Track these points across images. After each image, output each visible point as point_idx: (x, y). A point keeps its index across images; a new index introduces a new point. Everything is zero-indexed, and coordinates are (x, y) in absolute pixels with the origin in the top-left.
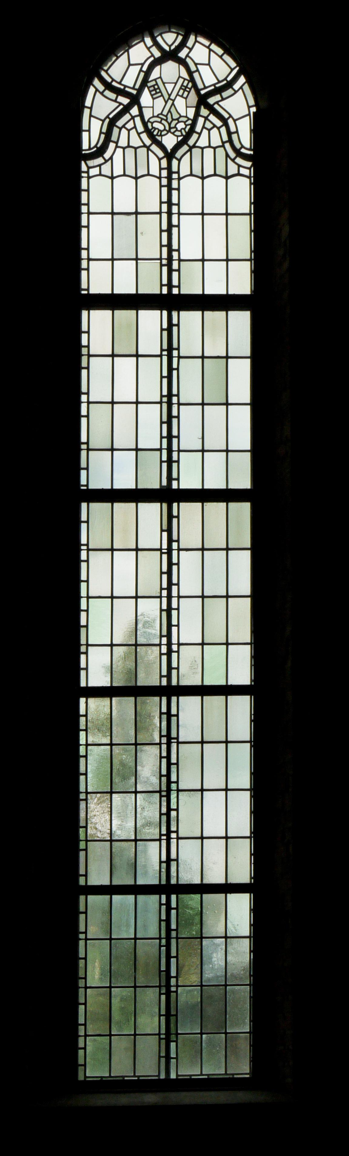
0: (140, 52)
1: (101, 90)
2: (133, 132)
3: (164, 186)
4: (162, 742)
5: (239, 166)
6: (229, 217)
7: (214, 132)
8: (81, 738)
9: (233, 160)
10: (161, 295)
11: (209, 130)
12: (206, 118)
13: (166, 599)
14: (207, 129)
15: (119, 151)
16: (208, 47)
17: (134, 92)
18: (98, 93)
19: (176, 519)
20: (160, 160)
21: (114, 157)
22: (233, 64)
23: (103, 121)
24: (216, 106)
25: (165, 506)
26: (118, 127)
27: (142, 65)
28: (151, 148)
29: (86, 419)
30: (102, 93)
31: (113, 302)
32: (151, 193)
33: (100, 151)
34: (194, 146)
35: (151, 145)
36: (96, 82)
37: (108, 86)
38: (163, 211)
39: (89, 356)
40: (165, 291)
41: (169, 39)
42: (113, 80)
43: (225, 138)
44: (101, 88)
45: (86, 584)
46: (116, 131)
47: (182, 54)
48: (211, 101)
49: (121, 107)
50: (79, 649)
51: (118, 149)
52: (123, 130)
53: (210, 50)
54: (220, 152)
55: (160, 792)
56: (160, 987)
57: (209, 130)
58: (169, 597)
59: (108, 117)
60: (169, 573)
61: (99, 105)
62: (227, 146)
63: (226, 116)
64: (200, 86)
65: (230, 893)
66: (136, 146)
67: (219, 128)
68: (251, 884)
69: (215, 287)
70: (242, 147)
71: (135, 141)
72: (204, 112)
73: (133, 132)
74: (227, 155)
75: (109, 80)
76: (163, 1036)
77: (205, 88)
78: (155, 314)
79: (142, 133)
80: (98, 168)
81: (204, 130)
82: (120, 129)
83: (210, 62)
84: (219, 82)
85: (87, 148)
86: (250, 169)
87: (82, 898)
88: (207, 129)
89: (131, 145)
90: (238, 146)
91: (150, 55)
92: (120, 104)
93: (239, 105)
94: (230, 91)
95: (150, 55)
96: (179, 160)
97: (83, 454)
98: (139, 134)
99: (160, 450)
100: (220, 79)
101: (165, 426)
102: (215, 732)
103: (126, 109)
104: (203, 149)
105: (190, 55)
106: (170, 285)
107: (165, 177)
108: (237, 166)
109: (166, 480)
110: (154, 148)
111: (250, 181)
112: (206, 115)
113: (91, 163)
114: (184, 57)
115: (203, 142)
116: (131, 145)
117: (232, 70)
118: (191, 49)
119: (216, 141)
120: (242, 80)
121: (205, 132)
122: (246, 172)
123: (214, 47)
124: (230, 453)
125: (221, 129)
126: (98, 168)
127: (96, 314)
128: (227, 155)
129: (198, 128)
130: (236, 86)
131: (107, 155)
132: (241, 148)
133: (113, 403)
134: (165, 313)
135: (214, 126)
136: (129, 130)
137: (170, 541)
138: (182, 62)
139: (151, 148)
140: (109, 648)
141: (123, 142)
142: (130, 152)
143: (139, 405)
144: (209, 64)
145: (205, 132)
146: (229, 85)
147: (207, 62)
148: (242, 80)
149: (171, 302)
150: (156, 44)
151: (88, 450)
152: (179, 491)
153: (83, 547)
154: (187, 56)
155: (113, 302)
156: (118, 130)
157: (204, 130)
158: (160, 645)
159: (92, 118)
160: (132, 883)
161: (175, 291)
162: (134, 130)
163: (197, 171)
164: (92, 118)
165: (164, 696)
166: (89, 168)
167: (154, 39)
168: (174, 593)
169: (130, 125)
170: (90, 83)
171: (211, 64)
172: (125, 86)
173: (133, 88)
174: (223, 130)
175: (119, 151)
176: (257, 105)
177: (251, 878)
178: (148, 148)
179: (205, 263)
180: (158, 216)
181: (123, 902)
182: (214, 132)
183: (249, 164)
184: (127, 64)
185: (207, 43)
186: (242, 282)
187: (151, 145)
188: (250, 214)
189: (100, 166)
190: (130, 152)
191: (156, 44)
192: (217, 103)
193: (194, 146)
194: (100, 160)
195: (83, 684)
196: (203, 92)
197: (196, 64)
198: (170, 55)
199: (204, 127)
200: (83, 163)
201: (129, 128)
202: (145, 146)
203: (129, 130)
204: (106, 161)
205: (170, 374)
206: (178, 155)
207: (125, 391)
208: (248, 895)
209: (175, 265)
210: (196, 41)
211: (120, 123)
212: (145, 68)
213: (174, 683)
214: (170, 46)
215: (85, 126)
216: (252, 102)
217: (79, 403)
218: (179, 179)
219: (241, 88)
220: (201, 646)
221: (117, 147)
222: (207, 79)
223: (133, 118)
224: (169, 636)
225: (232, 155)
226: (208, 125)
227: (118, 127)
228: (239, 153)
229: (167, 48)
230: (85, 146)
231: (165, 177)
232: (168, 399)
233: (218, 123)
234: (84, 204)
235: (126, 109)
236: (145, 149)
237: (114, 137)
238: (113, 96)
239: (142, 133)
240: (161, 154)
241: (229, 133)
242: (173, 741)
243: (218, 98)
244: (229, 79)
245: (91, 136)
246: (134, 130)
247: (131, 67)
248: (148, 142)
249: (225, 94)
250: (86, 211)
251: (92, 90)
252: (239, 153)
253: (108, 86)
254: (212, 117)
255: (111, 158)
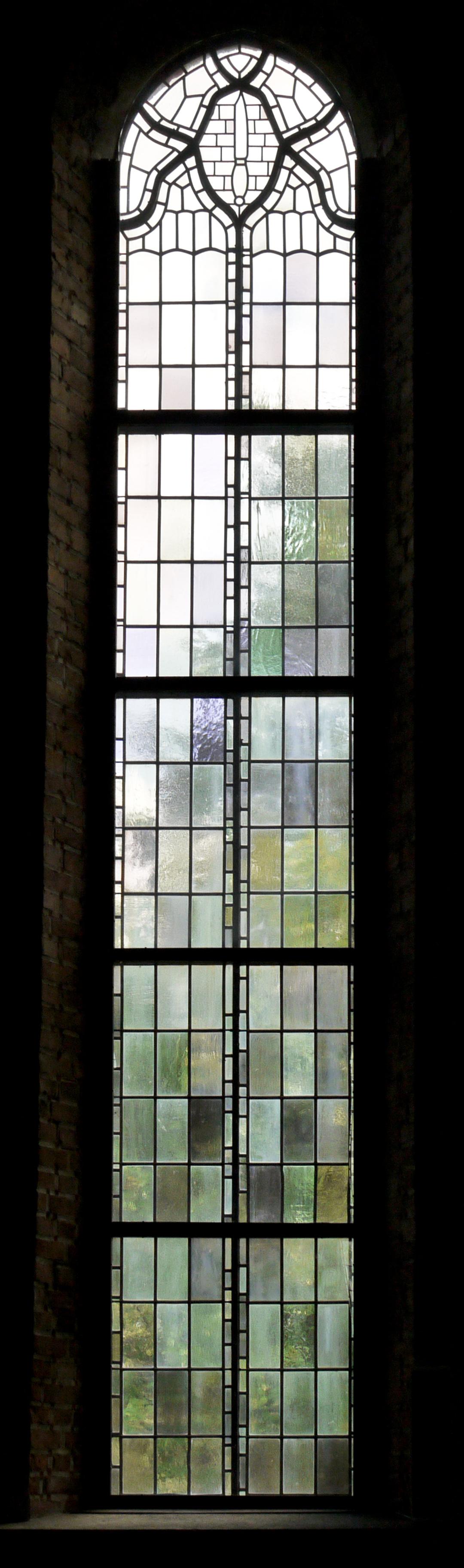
0: (200, 78)
1: (146, 130)
2: (188, 191)
3: (232, 263)
4: (229, 495)
5: (336, 236)
6: (155, 623)
7: (302, 192)
8: (113, 1342)
9: (328, 229)
10: (227, 412)
11: (295, 189)
12: (291, 171)
13: (232, 564)
14: (291, 187)
15: (170, 218)
16: (293, 74)
17: (192, 135)
18: (141, 134)
19: (249, 269)
20: (226, 229)
21: (163, 221)
22: (326, 98)
23: (149, 173)
24: (303, 155)
25: (230, 702)
26: (167, 183)
27: (204, 96)
28: (214, 212)
29: (125, 331)
30: (147, 134)
31: (159, 422)
32: (213, 274)
33: (143, 217)
34: (272, 211)
35: (214, 208)
36: (139, 119)
37: (155, 126)
38: (227, 1028)
39: (127, 366)
40: (232, 406)
41: (240, 60)
42: (163, 118)
43: (317, 200)
44: (146, 127)
45: (124, 384)
46: (164, 187)
47: (256, 83)
48: (296, 147)
49: (175, 154)
50: (111, 1101)
51: (167, 214)
52: (173, 187)
53: (296, 79)
54: (309, 220)
55: (226, 302)
56: (223, 1437)
57: (295, 189)
58: (237, 828)
59: (155, 168)
60: (239, 342)
61: (141, 153)
62: (320, 210)
63: (317, 167)
64: (282, 128)
65: (322, 1237)
66: (193, 209)
67: (308, 186)
68: (350, 677)
69: (300, 400)
70: (339, 209)
71: (192, 203)
72: (288, 162)
73: (188, 191)
74: (319, 223)
75: (157, 118)
76: (231, 304)
77: (288, 130)
78: (217, 440)
79: (200, 191)
80: (141, 239)
81: (287, 188)
82: (170, 185)
83: (297, 92)
84: (306, 121)
85: (125, 211)
86: (350, 240)
87: (116, 1241)
88: (291, 187)
89: (185, 208)
90: (333, 208)
91: (213, 84)
92: (174, 149)
93: (336, 152)
94: (323, 133)
95: (213, 84)
96: (252, 229)
97: (120, 567)
98: (196, 193)
99: (226, 366)
100: (307, 118)
101: (232, 384)
102: (303, 290)
103: (181, 158)
104: (284, 214)
105: (267, 83)
106: (236, 938)
107: (230, 1030)
108: (332, 237)
109: (232, 711)
110: (218, 212)
111: (350, 631)
112: (290, 166)
113: (130, 233)
114: (258, 86)
115: (286, 203)
116: (185, 208)
117: (324, 106)
118: (269, 75)
119: (303, 204)
120: (339, 117)
121: (289, 192)
122: (344, 246)
123: (300, 74)
124: (321, 307)
125: (311, 187)
126: (141, 239)
127: (136, 440)
128: (319, 223)
129: (279, 186)
130: (331, 126)
131: (153, 221)
132: (337, 211)
133: (158, 627)
134: (231, 438)
135: (303, 183)
136: (182, 188)
137: (237, 882)
138: (257, 93)
139: (214, 212)
140: (156, 565)
141: (174, 204)
142: (185, 218)
143: (197, 306)
144: (293, 97)
145: (289, 191)
146: (321, 124)
147: (291, 95)
148: (339, 117)
149: (236, 956)
150: (221, 69)
151: (126, 562)
152: (248, 950)
153: (118, 623)
154: (264, 84)
155: (159, 422)
156: (167, 186)
157: (287, 188)
158: (226, 366)
159: (132, 169)
160: (185, 1220)
161: (243, 944)
162: (190, 187)
163: (276, 245)
164: (132, 169)
165: (228, 1237)
166: (128, 240)
167: (217, 62)
168: (243, 821)
169: (184, 181)
170: (130, 121)
171: (296, 98)
172: (179, 126)
173: (191, 129)
174: (314, 188)
175: (170, 218)
176: (359, 151)
177: (351, 404)
178: (210, 212)
179: (287, 370)
180: (223, 565)
181: (174, 977)
182: (302, 192)
183: (349, 234)
184: (183, 97)
185: (291, 67)
186: (338, 393)
187: (214, 208)
188: (349, 1031)
189: (143, 237)
190: (185, 218)
191: (221, 69)
192: (304, 149)
193: (272, 211)
194: (144, 229)
195: (117, 945)
196: (285, 136)
197: (276, 96)
198: (241, 85)
199: (287, 185)
200: (121, 235)
201: (183, 185)
202: (205, 209)
203: (182, 188)
204: (152, 229)
205: (237, 340)
206: (250, 221)
207: (176, 482)
208: (347, 699)
209: (246, 310)
210: (275, 65)
211: (170, 178)
212: (206, 102)
213: (244, 673)
214: (239, 73)
215: (123, 181)
216: (351, 148)
217: (112, 894)
218: (252, 256)
219: (338, 128)
220: (282, 307)
221: (166, 211)
222: (291, 118)
223: (188, 170)
224: (239, 317)
225: (327, 222)
226: (294, 182)
227: (167, 183)
228: (336, 219)
229: (236, 75)
230: (123, 209)
231: (230, 1030)
232: (232, 1441)
233: (308, 179)
234: (122, 355)
235: (181, 158)
236: (207, 214)
237: (162, 198)
238: (163, 138)
239: (200, 191)
240: (228, 221)
241: (322, 191)
242: (242, 496)
243: (305, 142)
244: (319, 118)
245: (131, 197)
246: (190, 187)
247: (187, 100)
248: (210, 204)
249: (315, 137)
250: (124, 364)
251: (133, 131)
252: (336, 219)
253: (155, 126)
254: (299, 170)
255: (160, 223)
